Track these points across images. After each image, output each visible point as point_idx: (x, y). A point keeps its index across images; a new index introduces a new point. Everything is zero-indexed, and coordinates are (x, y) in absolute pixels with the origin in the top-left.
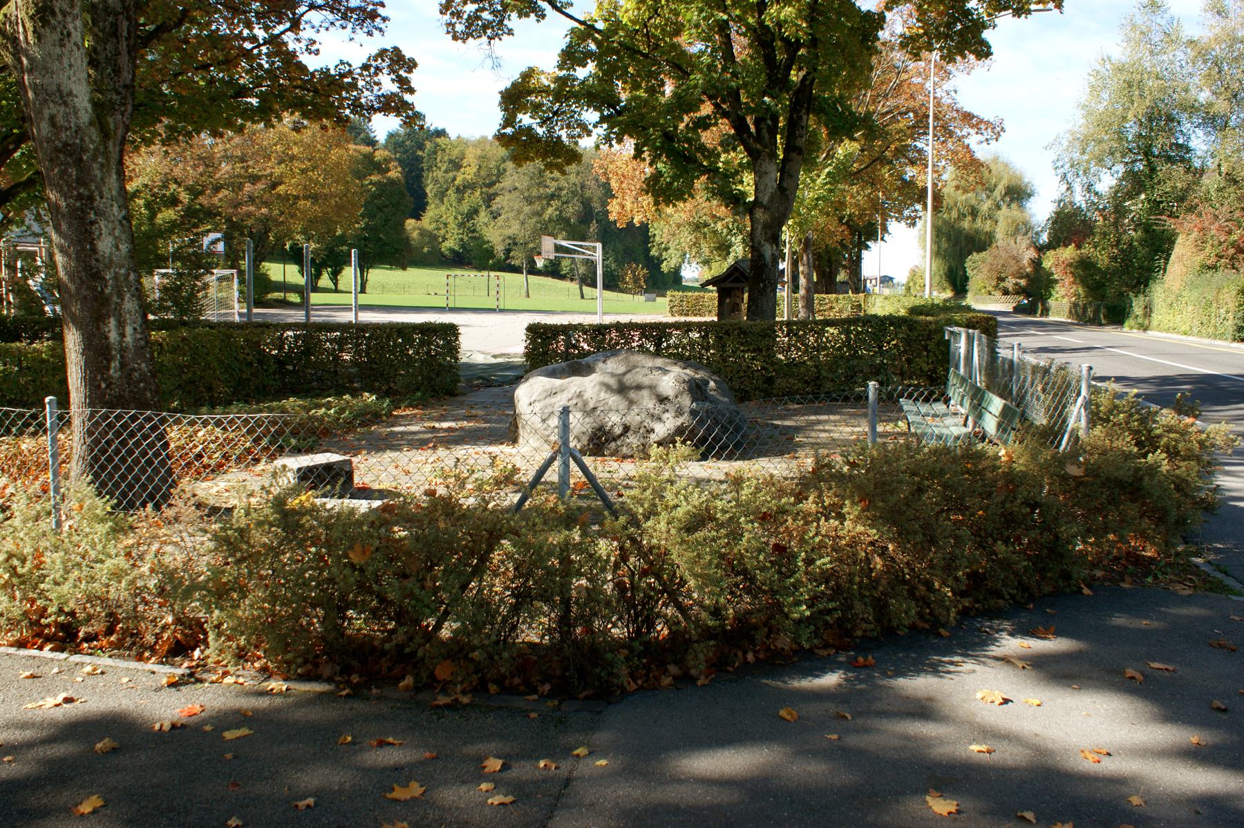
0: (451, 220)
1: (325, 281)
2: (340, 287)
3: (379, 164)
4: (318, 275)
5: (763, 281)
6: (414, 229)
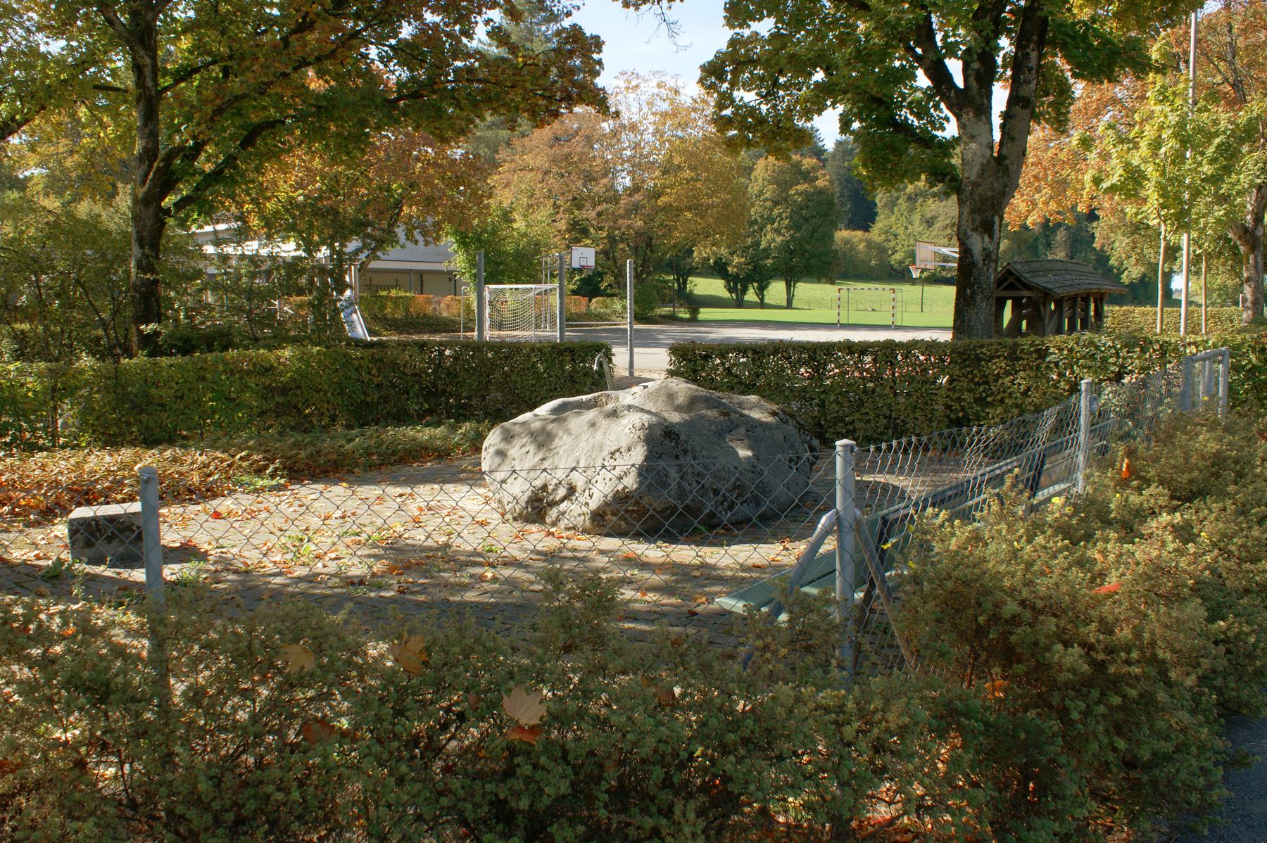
0: (900, 231)
1: (751, 296)
2: (767, 300)
3: (808, 172)
4: (744, 291)
5: (971, 286)
6: (861, 241)
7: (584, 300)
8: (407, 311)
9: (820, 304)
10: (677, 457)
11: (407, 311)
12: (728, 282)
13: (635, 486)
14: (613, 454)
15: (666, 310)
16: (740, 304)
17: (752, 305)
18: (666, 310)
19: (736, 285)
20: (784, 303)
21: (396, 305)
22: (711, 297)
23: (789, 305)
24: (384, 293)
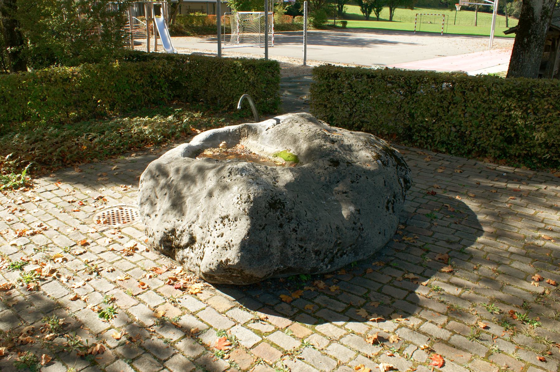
1: (373, 15)
2: (380, 17)
4: (370, 12)
5: (528, 36)
7: (291, 18)
8: (204, 23)
9: (405, 19)
10: (281, 226)
11: (204, 23)
12: (362, 8)
13: (236, 261)
14: (223, 218)
15: (331, 21)
16: (367, 18)
17: (373, 19)
18: (331, 21)
19: (366, 9)
20: (388, 19)
21: (198, 21)
22: (354, 15)
23: (391, 20)
24: (192, 14)
